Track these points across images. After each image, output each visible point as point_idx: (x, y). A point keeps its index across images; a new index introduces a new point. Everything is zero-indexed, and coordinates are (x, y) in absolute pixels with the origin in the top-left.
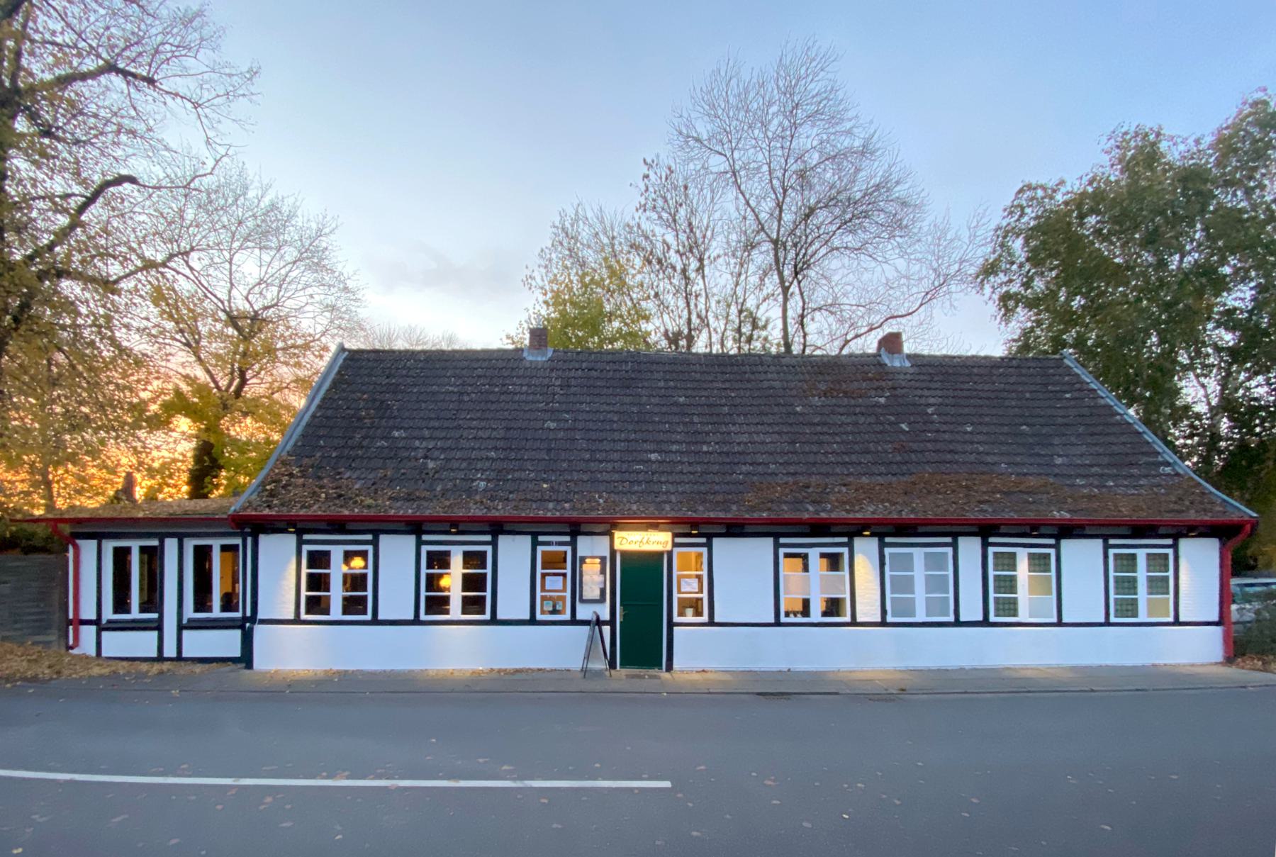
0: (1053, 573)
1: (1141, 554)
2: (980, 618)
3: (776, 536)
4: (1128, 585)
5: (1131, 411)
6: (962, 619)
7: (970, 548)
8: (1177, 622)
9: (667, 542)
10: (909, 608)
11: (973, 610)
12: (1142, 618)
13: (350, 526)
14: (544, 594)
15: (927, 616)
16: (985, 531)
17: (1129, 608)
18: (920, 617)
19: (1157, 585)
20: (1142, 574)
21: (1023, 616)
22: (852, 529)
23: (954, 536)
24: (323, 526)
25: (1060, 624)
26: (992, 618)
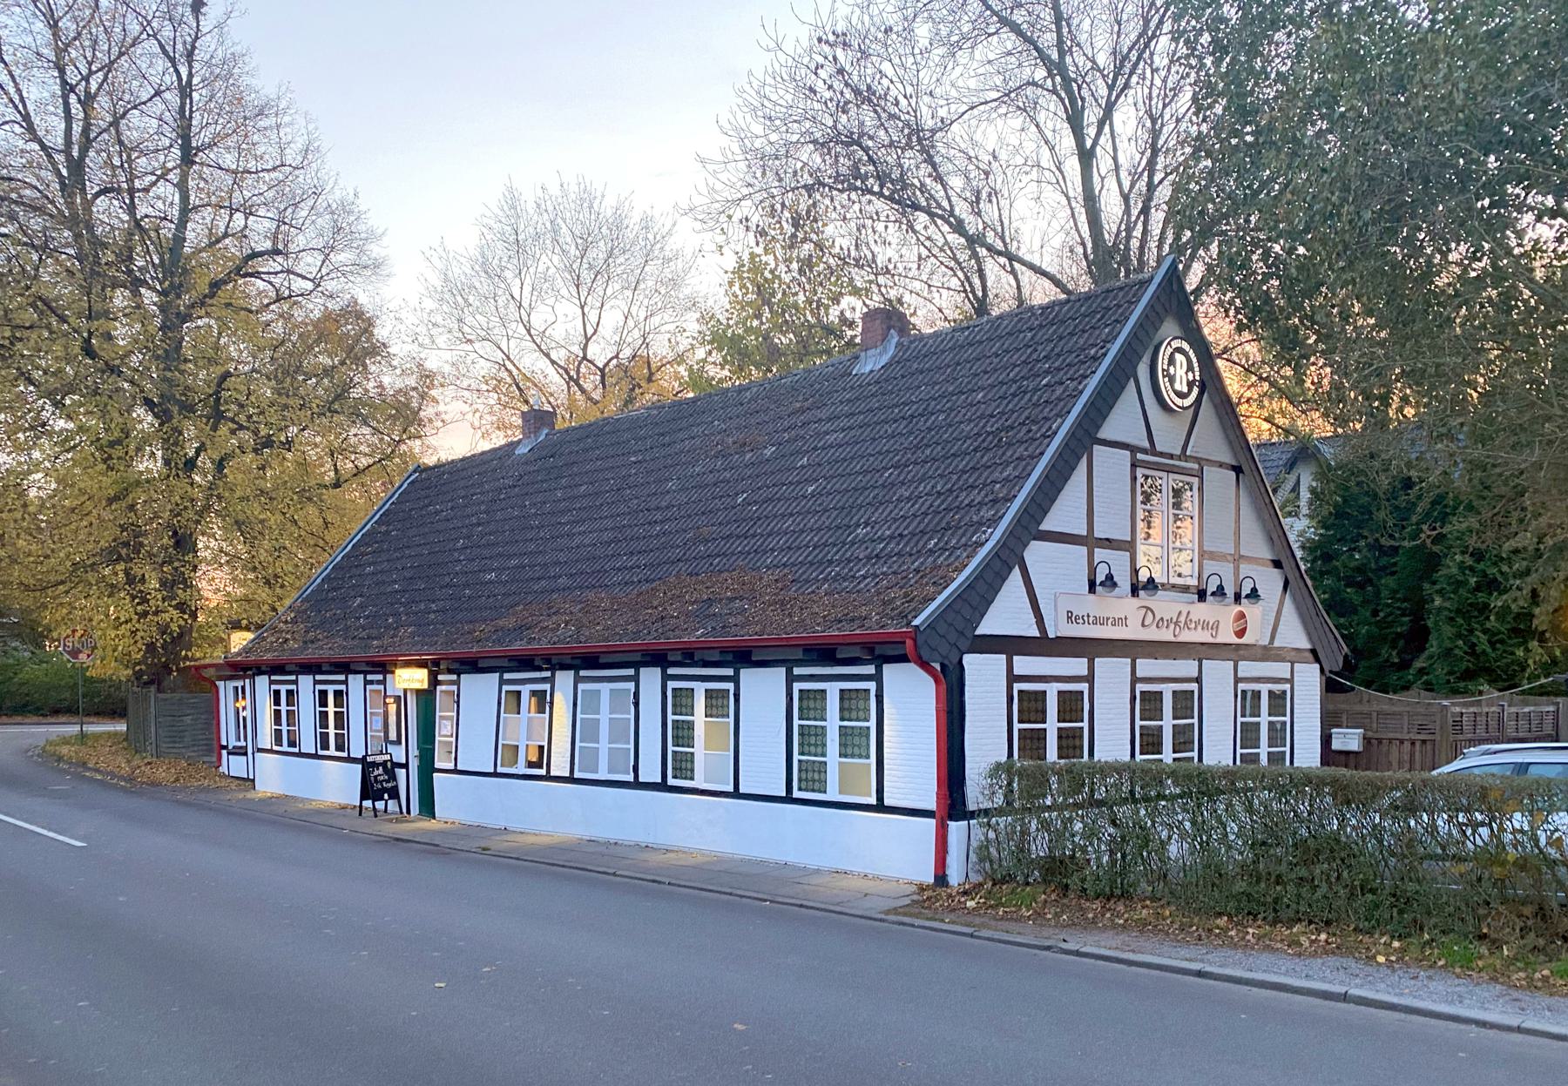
0: (731, 719)
1: (833, 690)
2: (784, 794)
3: (789, 664)
4: (813, 739)
5: (221, 576)
6: (887, 802)
7: (651, 677)
8: (880, 807)
9: (422, 681)
10: (592, 760)
11: (650, 773)
12: (832, 794)
13: (288, 668)
14: (803, 758)
15: (840, 793)
16: (658, 658)
17: (814, 776)
18: (602, 775)
19: (851, 743)
20: (833, 722)
21: (698, 782)
22: (637, 657)
23: (881, 660)
24: (716, 657)
25: (736, 794)
26: (796, 794)
